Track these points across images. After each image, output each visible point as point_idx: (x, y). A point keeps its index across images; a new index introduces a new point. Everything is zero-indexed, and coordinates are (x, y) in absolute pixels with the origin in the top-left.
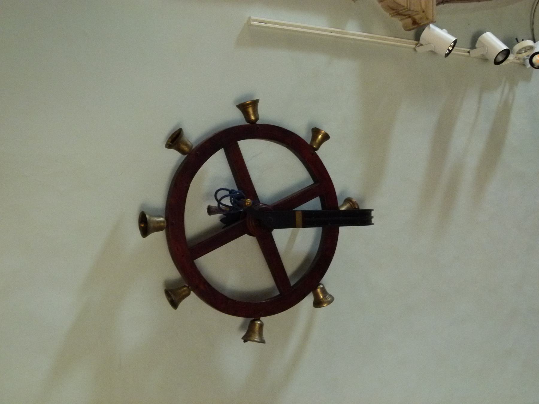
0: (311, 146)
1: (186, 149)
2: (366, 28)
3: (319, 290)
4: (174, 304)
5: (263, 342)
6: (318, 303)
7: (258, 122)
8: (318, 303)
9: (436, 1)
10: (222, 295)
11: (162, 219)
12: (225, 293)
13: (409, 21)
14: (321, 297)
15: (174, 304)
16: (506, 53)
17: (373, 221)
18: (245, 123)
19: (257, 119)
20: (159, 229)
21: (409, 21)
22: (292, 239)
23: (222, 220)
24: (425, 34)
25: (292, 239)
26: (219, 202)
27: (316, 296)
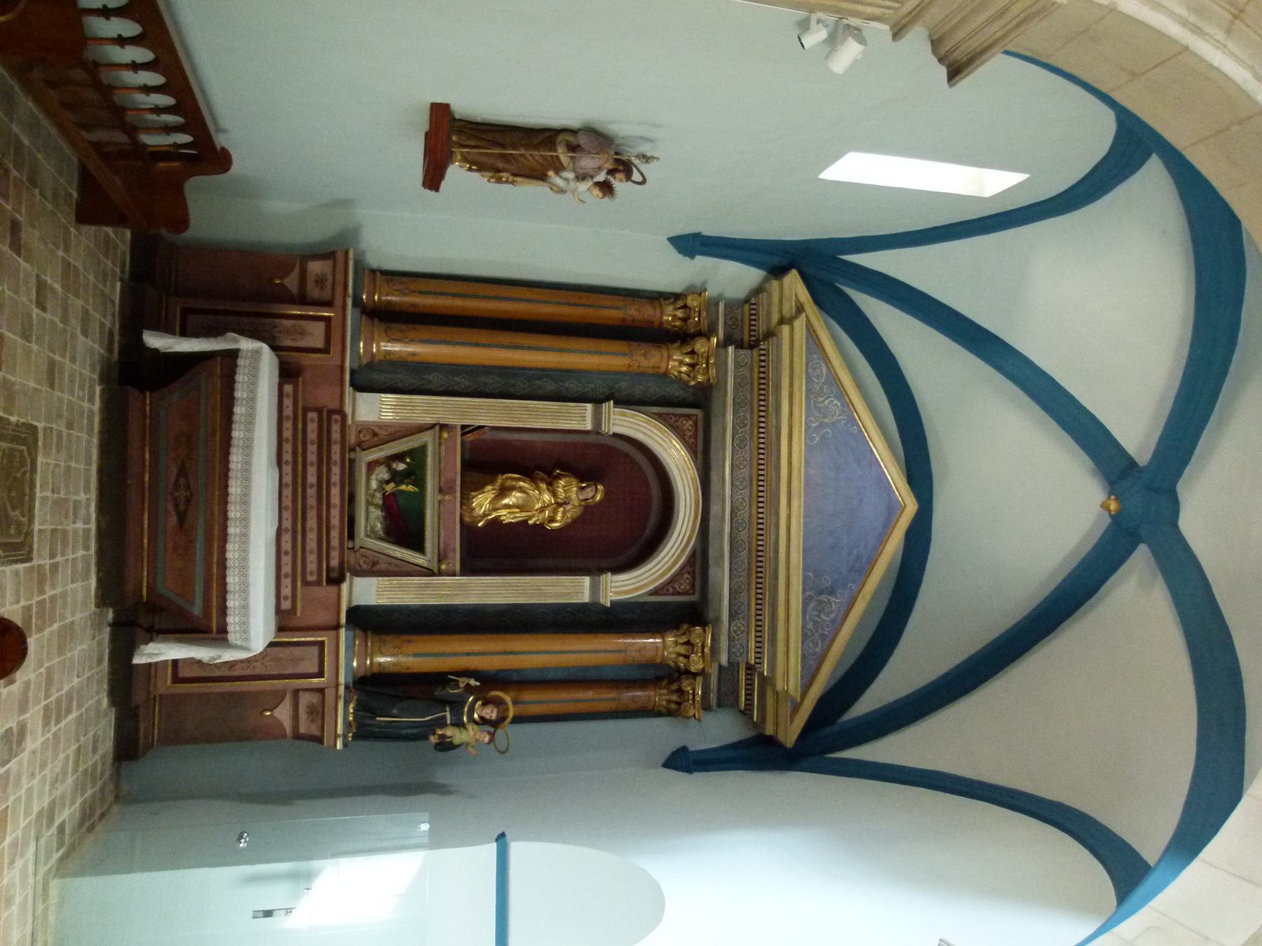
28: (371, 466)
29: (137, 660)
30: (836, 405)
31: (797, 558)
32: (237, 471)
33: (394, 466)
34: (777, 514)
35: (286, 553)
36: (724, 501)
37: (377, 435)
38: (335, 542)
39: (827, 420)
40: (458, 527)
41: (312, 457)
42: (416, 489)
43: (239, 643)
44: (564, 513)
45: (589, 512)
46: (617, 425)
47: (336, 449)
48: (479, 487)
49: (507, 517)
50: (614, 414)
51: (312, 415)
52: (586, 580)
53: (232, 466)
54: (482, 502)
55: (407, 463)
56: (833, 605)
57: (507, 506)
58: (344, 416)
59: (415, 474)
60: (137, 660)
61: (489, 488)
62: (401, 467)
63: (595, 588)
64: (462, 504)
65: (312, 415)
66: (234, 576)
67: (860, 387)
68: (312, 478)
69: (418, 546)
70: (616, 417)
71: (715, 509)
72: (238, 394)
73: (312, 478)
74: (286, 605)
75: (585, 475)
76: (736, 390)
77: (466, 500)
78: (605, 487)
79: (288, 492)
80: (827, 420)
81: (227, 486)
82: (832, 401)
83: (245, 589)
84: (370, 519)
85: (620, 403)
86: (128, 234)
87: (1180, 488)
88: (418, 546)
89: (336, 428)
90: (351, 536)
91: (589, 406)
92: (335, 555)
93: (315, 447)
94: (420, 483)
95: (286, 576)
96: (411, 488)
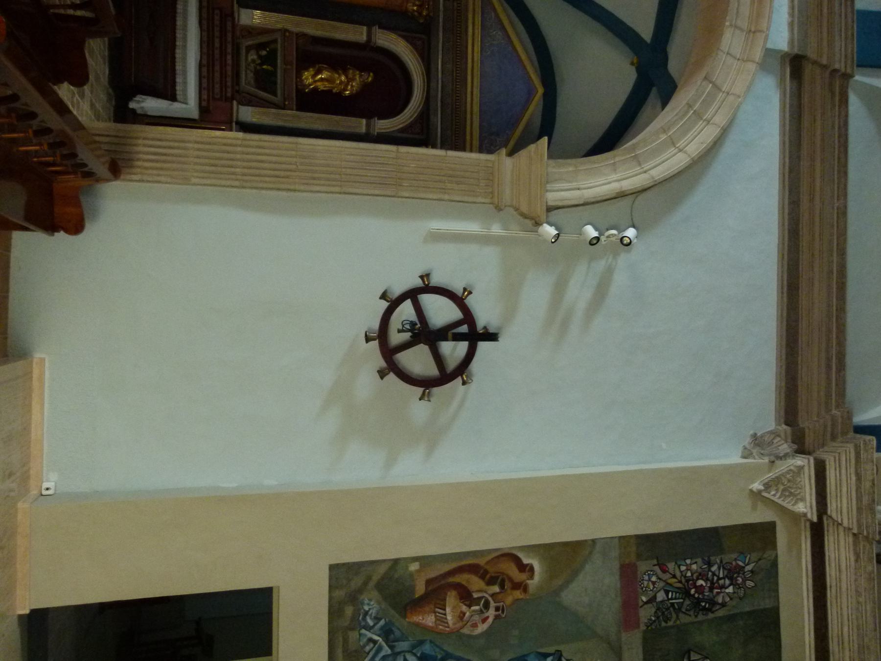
0: (462, 298)
1: (389, 300)
2: (506, 228)
3: (796, 493)
4: (382, 378)
5: (429, 401)
6: (464, 383)
7: (430, 285)
8: (464, 383)
9: (5, 368)
10: (411, 378)
11: (375, 335)
12: (413, 377)
13: (533, 221)
14: (465, 379)
15: (382, 378)
16: (598, 239)
17: (499, 339)
18: (423, 285)
19: (429, 284)
20: (374, 340)
21: (533, 221)
22: (454, 349)
23: (411, 337)
24: (541, 229)
25: (454, 349)
26: (403, 326)
27: (463, 379)
28: (249, 49)
29: (132, 105)
30: (499, 35)
31: (476, 109)
32: (180, 9)
33: (260, 53)
34: (466, 89)
35: (204, 77)
36: (438, 81)
37: (251, 31)
38: (229, 84)
39: (494, 42)
40: (294, 91)
41: (217, 34)
42: (272, 69)
43: (182, 100)
44: (352, 86)
45: (365, 87)
46: (381, 39)
47: (229, 35)
48: (307, 69)
49: (321, 86)
50: (379, 33)
51: (217, 12)
52: (364, 121)
53: (177, 56)
54: (308, 77)
55: (267, 51)
56: (498, 142)
57: (322, 80)
58: (234, 18)
59: (271, 59)
60: (132, 105)
61: (311, 69)
62: (264, 53)
63: (368, 126)
64: (296, 78)
65: (217, 12)
66: (179, 66)
67: (517, 34)
68: (217, 45)
69: (274, 94)
70: (380, 34)
71: (433, 84)
72: (178, 43)
73: (217, 45)
74: (204, 104)
75: (362, 67)
76: (444, 22)
77: (299, 75)
78: (374, 74)
79: (205, 46)
80: (494, 42)
81: (175, 33)
82: (497, 32)
83: (185, 73)
84: (247, 80)
85: (382, 27)
86: (106, 39)
87: (668, 49)
88: (274, 94)
89: (229, 24)
90: (238, 84)
91: (365, 28)
92: (229, 90)
93: (218, 29)
94: (275, 66)
95: (204, 88)
96: (269, 68)
